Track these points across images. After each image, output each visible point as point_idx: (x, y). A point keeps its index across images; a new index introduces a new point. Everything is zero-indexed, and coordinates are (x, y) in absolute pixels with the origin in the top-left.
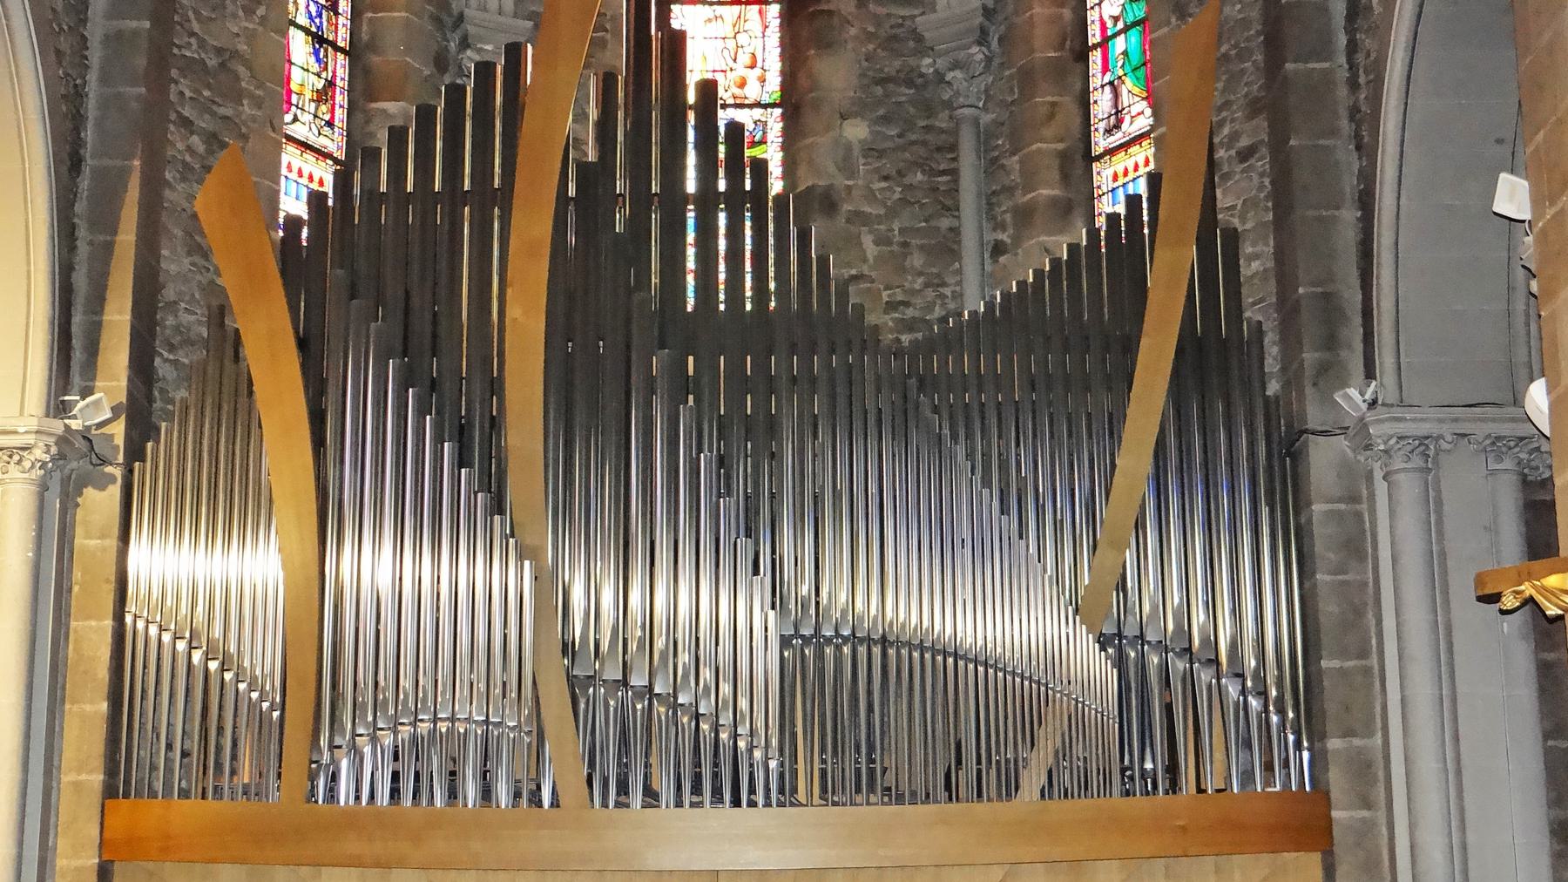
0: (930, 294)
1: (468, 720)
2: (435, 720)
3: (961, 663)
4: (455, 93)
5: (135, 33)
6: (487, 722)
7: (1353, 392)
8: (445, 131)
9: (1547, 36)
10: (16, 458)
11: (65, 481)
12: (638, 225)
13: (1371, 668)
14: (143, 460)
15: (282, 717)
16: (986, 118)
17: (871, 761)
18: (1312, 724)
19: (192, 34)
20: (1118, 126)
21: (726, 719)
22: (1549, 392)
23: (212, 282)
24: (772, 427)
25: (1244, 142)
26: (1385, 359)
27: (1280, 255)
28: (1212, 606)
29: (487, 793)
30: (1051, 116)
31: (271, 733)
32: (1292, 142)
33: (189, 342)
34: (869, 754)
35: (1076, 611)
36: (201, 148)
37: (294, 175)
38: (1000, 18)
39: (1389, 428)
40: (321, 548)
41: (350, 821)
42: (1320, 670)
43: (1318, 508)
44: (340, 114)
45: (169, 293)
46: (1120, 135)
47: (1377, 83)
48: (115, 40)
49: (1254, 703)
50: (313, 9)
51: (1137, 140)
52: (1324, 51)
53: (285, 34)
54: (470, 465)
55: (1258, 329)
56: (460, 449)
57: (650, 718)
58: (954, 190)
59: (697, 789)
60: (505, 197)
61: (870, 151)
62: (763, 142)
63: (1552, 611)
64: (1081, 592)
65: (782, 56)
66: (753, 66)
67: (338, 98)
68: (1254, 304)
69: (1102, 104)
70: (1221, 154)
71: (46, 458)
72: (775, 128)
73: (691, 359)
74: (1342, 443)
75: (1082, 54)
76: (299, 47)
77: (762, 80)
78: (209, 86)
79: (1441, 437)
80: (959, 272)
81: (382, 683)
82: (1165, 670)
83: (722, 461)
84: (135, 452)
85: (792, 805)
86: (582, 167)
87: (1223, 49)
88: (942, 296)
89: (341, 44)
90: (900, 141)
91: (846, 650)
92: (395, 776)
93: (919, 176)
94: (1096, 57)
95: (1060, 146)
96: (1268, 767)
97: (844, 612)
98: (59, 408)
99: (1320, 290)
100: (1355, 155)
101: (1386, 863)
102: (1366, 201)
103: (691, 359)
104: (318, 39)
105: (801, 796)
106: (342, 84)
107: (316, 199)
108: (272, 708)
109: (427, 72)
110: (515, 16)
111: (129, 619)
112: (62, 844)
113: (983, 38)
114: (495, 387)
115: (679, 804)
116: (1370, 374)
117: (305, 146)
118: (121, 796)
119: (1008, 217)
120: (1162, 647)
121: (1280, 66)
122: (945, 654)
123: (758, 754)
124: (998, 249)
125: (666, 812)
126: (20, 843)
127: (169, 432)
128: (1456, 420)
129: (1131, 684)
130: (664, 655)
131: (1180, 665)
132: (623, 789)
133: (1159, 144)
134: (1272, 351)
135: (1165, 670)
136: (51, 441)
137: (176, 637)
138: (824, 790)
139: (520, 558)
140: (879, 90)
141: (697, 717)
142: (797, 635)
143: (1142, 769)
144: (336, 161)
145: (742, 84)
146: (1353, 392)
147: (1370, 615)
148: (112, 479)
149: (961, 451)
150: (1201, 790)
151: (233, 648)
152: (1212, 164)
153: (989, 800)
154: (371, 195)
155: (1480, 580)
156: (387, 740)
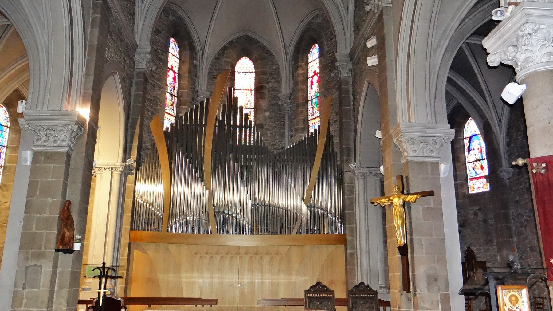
0: (279, 143)
1: (196, 218)
2: (190, 218)
4: (197, 107)
5: (140, 94)
6: (199, 219)
7: (352, 165)
8: (195, 114)
9: (385, 108)
11: (125, 174)
12: (229, 130)
13: (354, 213)
16: (290, 112)
17: (267, 227)
18: (343, 222)
19: (149, 94)
20: (313, 115)
23: (151, 138)
24: (251, 167)
25: (335, 119)
26: (358, 159)
27: (341, 140)
28: (327, 201)
29: (199, 231)
30: (301, 113)
31: (160, 220)
33: (148, 149)
34: (266, 225)
35: (303, 201)
36: (150, 114)
38: (293, 95)
39: (358, 171)
41: (175, 236)
44: (175, 108)
45: (144, 140)
47: (358, 111)
48: (136, 96)
49: (334, 218)
52: (349, 104)
56: (196, 170)
58: (284, 125)
59: (236, 231)
61: (269, 117)
64: (304, 198)
65: (254, 100)
67: (175, 105)
69: (310, 111)
70: (331, 121)
71: (122, 170)
72: (253, 113)
75: (307, 102)
76: (168, 96)
77: (251, 104)
78: (152, 103)
80: (285, 139)
82: (318, 211)
83: (242, 173)
84: (138, 169)
85: (253, 234)
88: (282, 144)
89: (175, 95)
90: (275, 116)
94: (310, 103)
96: (336, 229)
97: (263, 200)
98: (124, 161)
100: (354, 123)
102: (355, 131)
104: (172, 95)
105: (254, 233)
107: (172, 125)
108: (161, 215)
111: (135, 199)
112: (122, 239)
113: (290, 98)
114: (202, 159)
115: (233, 234)
116: (355, 161)
120: (318, 208)
121: (341, 107)
122: (280, 208)
123: (247, 225)
124: (292, 136)
128: (369, 170)
131: (321, 211)
132: (223, 231)
133: (320, 118)
134: (339, 155)
135: (318, 211)
137: (144, 202)
138: (258, 232)
139: (206, 189)
141: (236, 219)
143: (314, 229)
146: (352, 165)
149: (284, 172)
150: (324, 233)
151: (154, 204)
152: (329, 123)
153: (287, 234)
154: (181, 124)
155: (371, 200)
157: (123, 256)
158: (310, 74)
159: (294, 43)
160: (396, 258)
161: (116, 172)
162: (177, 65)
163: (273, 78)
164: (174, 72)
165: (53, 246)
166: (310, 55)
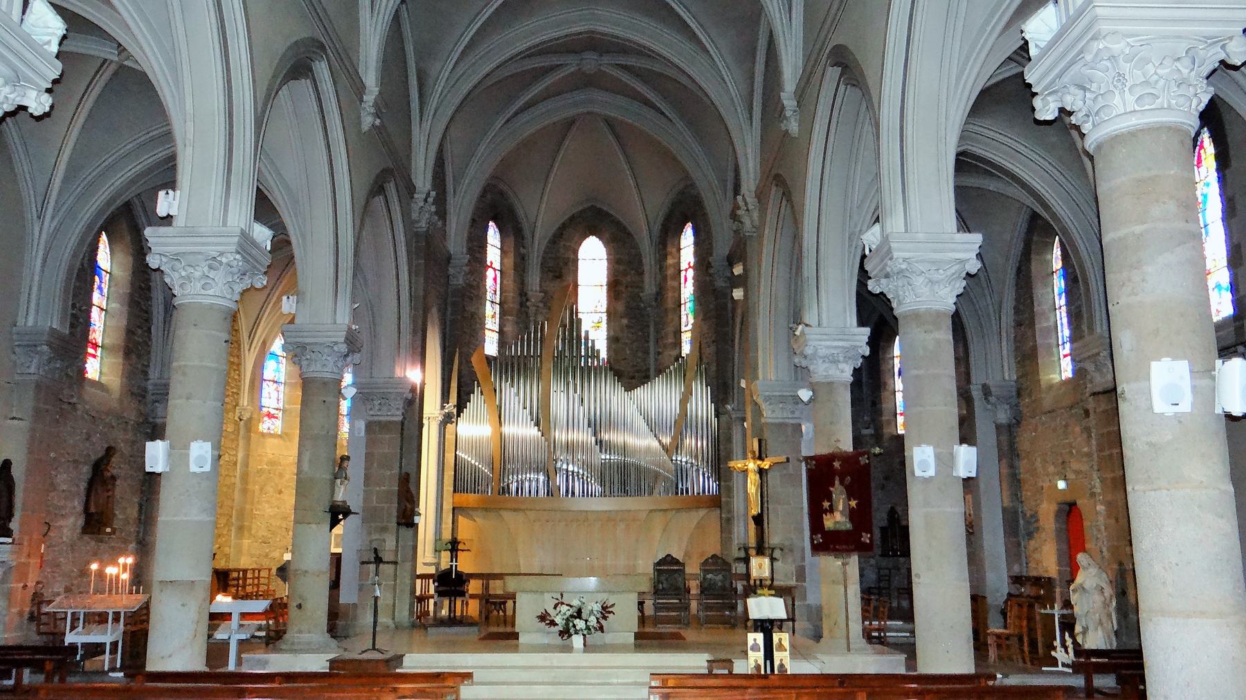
40: (961, 349)
94: (683, 306)
98: (443, 407)
106: (498, 312)
118: (122, 615)
124: (659, 353)
157: (446, 524)
158: (684, 266)
159: (660, 220)
160: (752, 526)
161: (434, 422)
162: (498, 259)
163: (633, 269)
164: (495, 270)
165: (395, 520)
166: (682, 237)
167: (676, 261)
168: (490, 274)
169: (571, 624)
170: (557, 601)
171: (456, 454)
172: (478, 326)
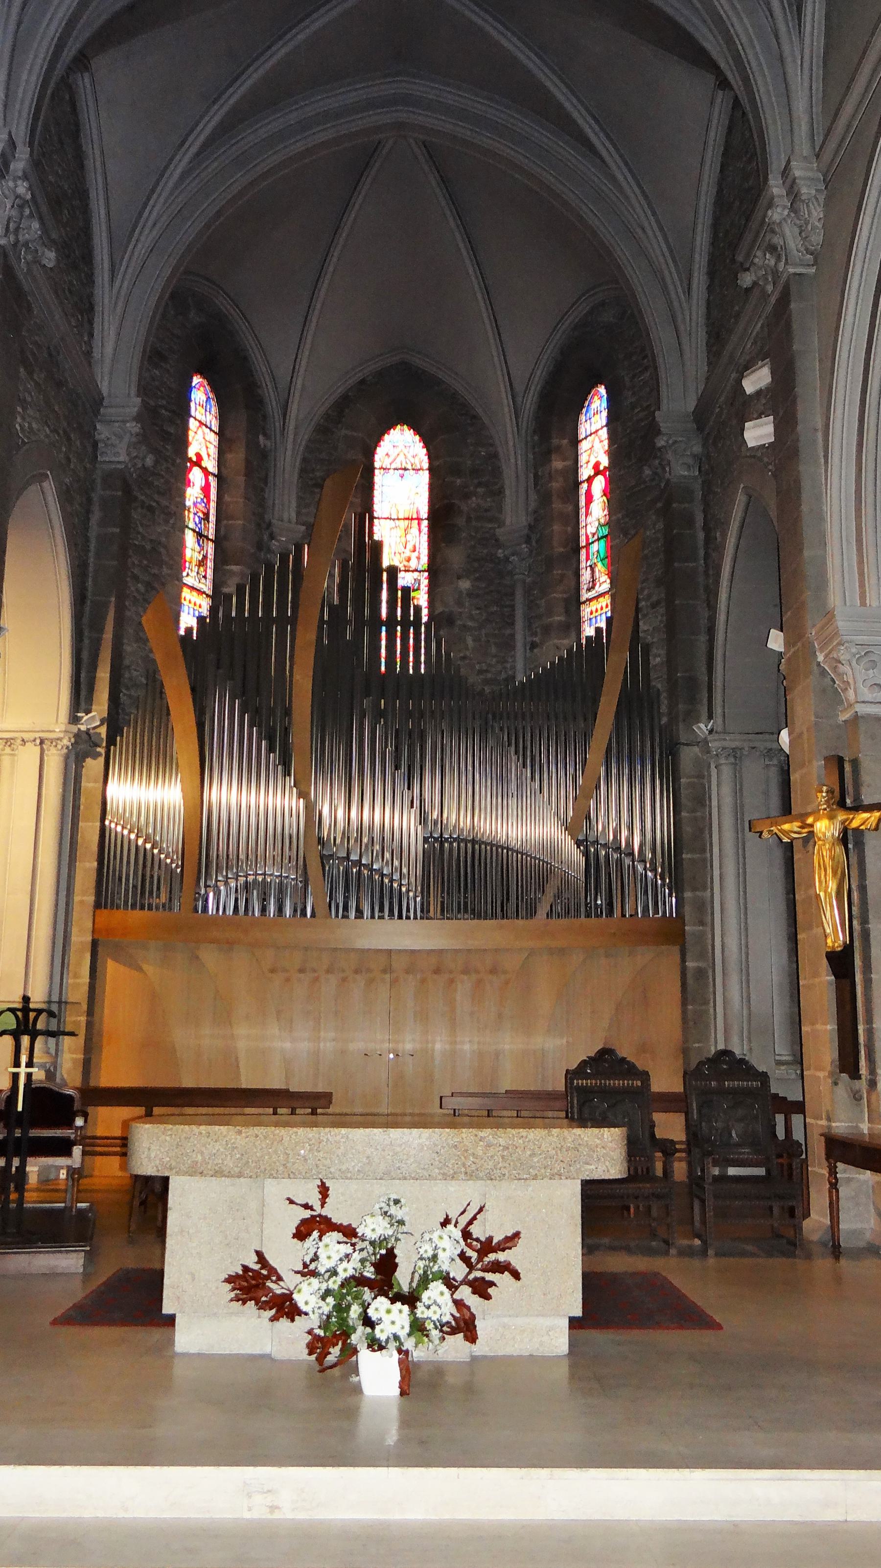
0: (499, 667)
3: (510, 853)
7: (702, 726)
10: (54, 744)
11: (77, 757)
14: (115, 745)
15: (182, 871)
16: (528, 580)
17: (465, 898)
18: (677, 886)
19: (139, 533)
20: (593, 587)
21: (396, 876)
22: (789, 735)
23: (148, 656)
25: (655, 598)
26: (718, 710)
28: (631, 829)
30: (561, 581)
31: (175, 880)
32: (677, 602)
35: (566, 829)
37: (192, 605)
42: (682, 859)
43: (683, 781)
44: (210, 573)
45: (127, 662)
46: (594, 592)
47: (718, 575)
49: (649, 874)
50: (197, 520)
51: (602, 595)
53: (183, 533)
54: (274, 752)
55: (658, 693)
57: (359, 877)
58: (512, 616)
59: (381, 910)
60: (293, 621)
61: (470, 595)
62: (418, 589)
63: (786, 840)
64: (569, 820)
66: (414, 551)
68: (658, 678)
70: (642, 604)
71: (69, 744)
72: (425, 582)
73: (383, 701)
74: (696, 749)
76: (190, 538)
77: (418, 558)
79: (743, 748)
80: (514, 656)
81: (231, 857)
84: (111, 741)
85: (427, 919)
86: (331, 607)
87: (646, 552)
88: (505, 668)
89: (210, 537)
91: (455, 844)
92: (236, 900)
93: (495, 608)
94: (583, 552)
95: (565, 596)
97: (455, 827)
98: (74, 719)
99: (687, 674)
101: (710, 951)
102: (711, 631)
103: (383, 701)
104: (200, 535)
105: (431, 914)
108: (177, 867)
109: (252, 551)
110: (297, 523)
111: (107, 823)
112: (75, 930)
115: (373, 917)
117: (192, 588)
119: (538, 630)
120: (605, 846)
123: (411, 894)
124: (533, 646)
125: (366, 921)
126: (55, 929)
127: (128, 732)
129: (592, 865)
130: (367, 845)
132: (346, 908)
136: (72, 736)
137: (130, 832)
140: (476, 565)
142: (431, 836)
144: (208, 596)
145: (409, 560)
146: (702, 726)
147: (707, 832)
148: (100, 754)
152: (637, 610)
153: (522, 918)
156: (233, 884)
159: (540, 376)
161: (53, 751)
162: (213, 451)
163: (480, 484)
164: (205, 471)
166: (583, 418)
167: (568, 463)
168: (196, 476)
169: (355, 1311)
170: (307, 1214)
171: (103, 829)
172: (165, 570)
